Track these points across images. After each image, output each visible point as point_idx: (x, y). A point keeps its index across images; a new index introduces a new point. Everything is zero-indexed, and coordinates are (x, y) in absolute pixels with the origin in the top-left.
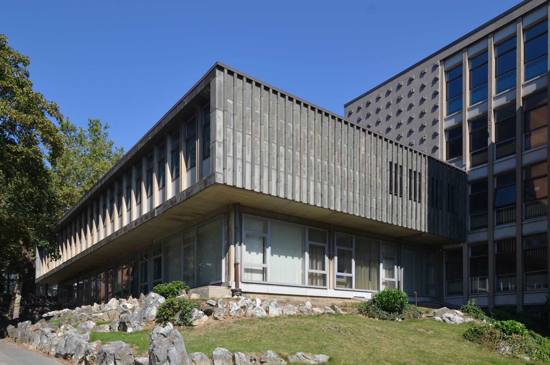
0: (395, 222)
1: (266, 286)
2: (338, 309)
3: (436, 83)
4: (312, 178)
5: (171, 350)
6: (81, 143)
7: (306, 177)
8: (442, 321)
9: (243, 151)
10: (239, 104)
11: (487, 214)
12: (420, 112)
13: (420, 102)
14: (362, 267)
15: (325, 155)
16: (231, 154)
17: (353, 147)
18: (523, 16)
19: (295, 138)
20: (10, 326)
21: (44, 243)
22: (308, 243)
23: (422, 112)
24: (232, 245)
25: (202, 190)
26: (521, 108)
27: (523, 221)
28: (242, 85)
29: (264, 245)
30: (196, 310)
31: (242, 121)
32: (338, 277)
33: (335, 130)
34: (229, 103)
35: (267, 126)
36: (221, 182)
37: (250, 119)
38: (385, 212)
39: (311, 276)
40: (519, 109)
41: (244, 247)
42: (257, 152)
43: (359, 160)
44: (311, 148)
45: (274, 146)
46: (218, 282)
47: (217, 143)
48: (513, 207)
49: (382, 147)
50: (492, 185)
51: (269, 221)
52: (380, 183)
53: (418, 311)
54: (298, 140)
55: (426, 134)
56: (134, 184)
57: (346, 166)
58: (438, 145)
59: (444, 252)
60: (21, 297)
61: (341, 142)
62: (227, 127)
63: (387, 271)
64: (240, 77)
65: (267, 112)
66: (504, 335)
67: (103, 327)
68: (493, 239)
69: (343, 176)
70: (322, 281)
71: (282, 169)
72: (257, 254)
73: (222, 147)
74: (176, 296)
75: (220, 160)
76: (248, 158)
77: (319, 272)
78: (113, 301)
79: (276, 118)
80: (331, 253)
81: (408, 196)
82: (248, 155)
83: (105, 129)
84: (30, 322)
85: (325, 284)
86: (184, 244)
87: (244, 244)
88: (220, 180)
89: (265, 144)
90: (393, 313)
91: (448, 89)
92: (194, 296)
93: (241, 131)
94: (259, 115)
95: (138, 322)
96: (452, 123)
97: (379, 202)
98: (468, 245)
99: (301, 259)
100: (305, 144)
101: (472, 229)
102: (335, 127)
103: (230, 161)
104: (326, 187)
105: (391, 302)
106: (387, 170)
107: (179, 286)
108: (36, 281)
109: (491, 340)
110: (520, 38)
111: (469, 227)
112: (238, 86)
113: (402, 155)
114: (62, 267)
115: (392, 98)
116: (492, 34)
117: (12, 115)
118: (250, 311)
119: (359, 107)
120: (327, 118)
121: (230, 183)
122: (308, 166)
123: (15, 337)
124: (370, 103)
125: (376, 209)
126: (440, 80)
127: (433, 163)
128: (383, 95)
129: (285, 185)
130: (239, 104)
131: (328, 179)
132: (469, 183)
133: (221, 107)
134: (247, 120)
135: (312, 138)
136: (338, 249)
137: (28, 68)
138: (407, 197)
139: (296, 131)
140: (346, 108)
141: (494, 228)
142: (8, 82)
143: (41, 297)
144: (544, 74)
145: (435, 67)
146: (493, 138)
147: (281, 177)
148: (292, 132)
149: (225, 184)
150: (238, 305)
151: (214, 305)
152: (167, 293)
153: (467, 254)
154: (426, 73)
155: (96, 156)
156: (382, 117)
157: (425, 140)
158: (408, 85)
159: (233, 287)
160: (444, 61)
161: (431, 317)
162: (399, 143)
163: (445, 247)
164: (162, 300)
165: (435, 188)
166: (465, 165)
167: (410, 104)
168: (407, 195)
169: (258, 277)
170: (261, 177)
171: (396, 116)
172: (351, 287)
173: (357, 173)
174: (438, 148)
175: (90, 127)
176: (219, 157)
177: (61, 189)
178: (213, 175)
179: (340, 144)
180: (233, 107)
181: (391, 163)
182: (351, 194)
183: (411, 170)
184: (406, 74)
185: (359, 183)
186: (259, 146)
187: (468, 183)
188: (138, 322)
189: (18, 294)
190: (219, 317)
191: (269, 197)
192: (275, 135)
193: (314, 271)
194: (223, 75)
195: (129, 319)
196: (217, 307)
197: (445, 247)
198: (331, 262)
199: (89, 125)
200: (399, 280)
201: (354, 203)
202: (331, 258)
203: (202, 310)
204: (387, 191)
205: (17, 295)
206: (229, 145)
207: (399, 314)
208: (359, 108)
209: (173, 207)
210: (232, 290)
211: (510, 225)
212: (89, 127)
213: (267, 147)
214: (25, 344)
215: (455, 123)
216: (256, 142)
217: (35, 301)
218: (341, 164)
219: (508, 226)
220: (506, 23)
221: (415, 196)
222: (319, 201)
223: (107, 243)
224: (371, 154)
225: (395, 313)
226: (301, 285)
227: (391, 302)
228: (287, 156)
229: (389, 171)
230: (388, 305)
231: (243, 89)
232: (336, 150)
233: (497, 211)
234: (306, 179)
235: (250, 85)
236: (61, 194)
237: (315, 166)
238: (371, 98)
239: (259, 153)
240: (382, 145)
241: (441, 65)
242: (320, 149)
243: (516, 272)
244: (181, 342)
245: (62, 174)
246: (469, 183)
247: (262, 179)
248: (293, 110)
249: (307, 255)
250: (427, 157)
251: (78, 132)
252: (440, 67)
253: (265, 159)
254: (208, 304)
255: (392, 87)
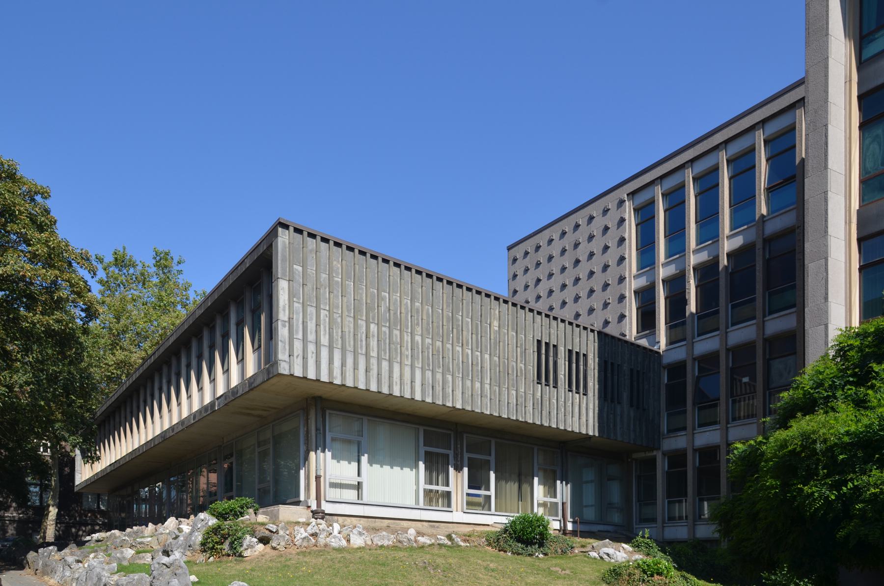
0: (547, 422)
1: (362, 507)
2: (455, 539)
3: (622, 225)
4: (418, 364)
5: (171, 581)
6: (144, 284)
7: (409, 363)
8: (599, 558)
9: (316, 332)
10: (311, 270)
11: (685, 412)
12: (603, 265)
13: (603, 250)
14: (506, 482)
15: (438, 334)
16: (300, 336)
17: (481, 321)
18: (727, 142)
19: (392, 312)
20: (31, 552)
21: (75, 440)
22: (423, 450)
23: (605, 264)
24: (312, 451)
25: (265, 381)
26: (726, 268)
27: (729, 424)
28: (315, 246)
29: (359, 452)
30: (248, 537)
31: (315, 293)
32: (468, 495)
33: (452, 299)
34: (297, 270)
35: (351, 297)
36: (286, 372)
37: (327, 289)
38: (530, 408)
39: (428, 493)
40: (722, 269)
41: (329, 454)
42: (337, 333)
43: (490, 339)
44: (418, 324)
45: (362, 323)
46: (296, 500)
47: (280, 323)
48: (753, 396)
49: (525, 320)
50: (692, 372)
51: (365, 419)
52: (523, 369)
53: (568, 544)
54: (397, 316)
55: (611, 295)
56: (194, 362)
57: (470, 347)
58: (625, 312)
59: (634, 462)
60: (57, 510)
61: (462, 316)
62: (294, 301)
63: (547, 488)
64: (312, 236)
65: (351, 280)
66: (644, 577)
67: (143, 557)
68: (693, 446)
69: (465, 361)
70: (446, 501)
71: (374, 354)
72: (350, 463)
73: (287, 328)
74: (238, 517)
75: (285, 344)
76: (325, 340)
77: (441, 488)
78: (172, 521)
79: (364, 287)
80: (459, 463)
81: (567, 387)
82: (325, 337)
83: (178, 265)
84: (56, 548)
85: (449, 505)
86: (259, 447)
87: (329, 451)
88: (285, 370)
89: (349, 321)
90: (531, 546)
91: (639, 234)
92: (261, 518)
93: (315, 305)
94: (340, 283)
95: (182, 551)
96: (642, 282)
97: (521, 395)
98: (664, 454)
99: (414, 470)
100: (408, 320)
101: (669, 431)
102: (453, 296)
103: (298, 345)
104: (439, 376)
105: (527, 531)
106: (534, 352)
107: (244, 504)
108: (76, 489)
109: (629, 583)
110: (723, 172)
111: (664, 428)
112: (310, 248)
113: (557, 331)
114: (109, 471)
115: (567, 242)
116: (690, 164)
117: (25, 272)
118: (322, 539)
119: (526, 251)
120: (441, 283)
121: (298, 372)
122: (411, 349)
123: (36, 568)
124: (540, 246)
125: (517, 405)
126: (627, 221)
127: (604, 338)
128: (555, 237)
129: (378, 374)
130: (311, 270)
131: (443, 366)
132: (664, 368)
133: (285, 276)
134: (321, 291)
135: (418, 312)
136: (469, 458)
137: (49, 203)
138: (565, 388)
139: (394, 304)
140: (510, 251)
141: (695, 432)
142: (20, 225)
143: (90, 511)
144: (791, 207)
145: (621, 202)
146: (692, 307)
147: (373, 365)
148: (388, 305)
149: (292, 375)
150: (306, 531)
151: (274, 531)
152: (226, 514)
153: (662, 466)
154: (609, 209)
155: (164, 307)
156: (555, 268)
157: (609, 303)
158: (587, 225)
159: (314, 507)
160: (632, 194)
161: (585, 552)
162: (552, 314)
163: (635, 456)
164: (213, 521)
165: (609, 375)
166: (659, 342)
167: (591, 252)
168: (565, 386)
169: (351, 495)
170: (343, 364)
171: (574, 268)
172: (490, 509)
173: (487, 356)
174: (625, 316)
175: (157, 261)
176: (283, 340)
177: (113, 354)
178: (276, 363)
179: (460, 318)
180: (303, 275)
181: (539, 342)
182: (478, 385)
183: (570, 351)
184: (586, 209)
185: (490, 369)
186: (340, 324)
187: (663, 367)
188: (182, 551)
189: (53, 506)
190: (278, 547)
191: (355, 390)
192: (363, 310)
193: (434, 487)
194: (287, 234)
195: (173, 546)
196: (278, 534)
197: (635, 456)
198: (459, 474)
199: (155, 258)
200: (564, 501)
201: (481, 397)
202: (458, 469)
203: (256, 537)
204: (533, 381)
205: (51, 508)
206: (297, 325)
207: (539, 547)
208: (527, 253)
209: (235, 399)
210: (312, 512)
211: (714, 428)
212: (154, 261)
213: (352, 325)
214: (46, 578)
215: (647, 282)
216: (336, 319)
217: (80, 517)
218: (462, 345)
219: (711, 429)
220: (706, 149)
221: (577, 384)
222: (428, 395)
223: (162, 441)
224: (508, 330)
225: (533, 547)
226: (413, 505)
227: (527, 531)
228: (380, 336)
229: (536, 354)
230: (523, 534)
231: (316, 251)
232: (455, 327)
233: (698, 408)
234: (410, 367)
235: (327, 245)
236: (114, 361)
237: (422, 348)
238: (542, 239)
239: (340, 334)
240: (525, 318)
241: (629, 200)
242: (431, 326)
243: (720, 494)
244: (185, 573)
245: (114, 331)
246: (664, 368)
247: (344, 368)
248: (389, 276)
249: (422, 465)
250: (596, 332)
251: (139, 268)
252: (627, 203)
253: (349, 342)
254: (267, 529)
255: (567, 225)
